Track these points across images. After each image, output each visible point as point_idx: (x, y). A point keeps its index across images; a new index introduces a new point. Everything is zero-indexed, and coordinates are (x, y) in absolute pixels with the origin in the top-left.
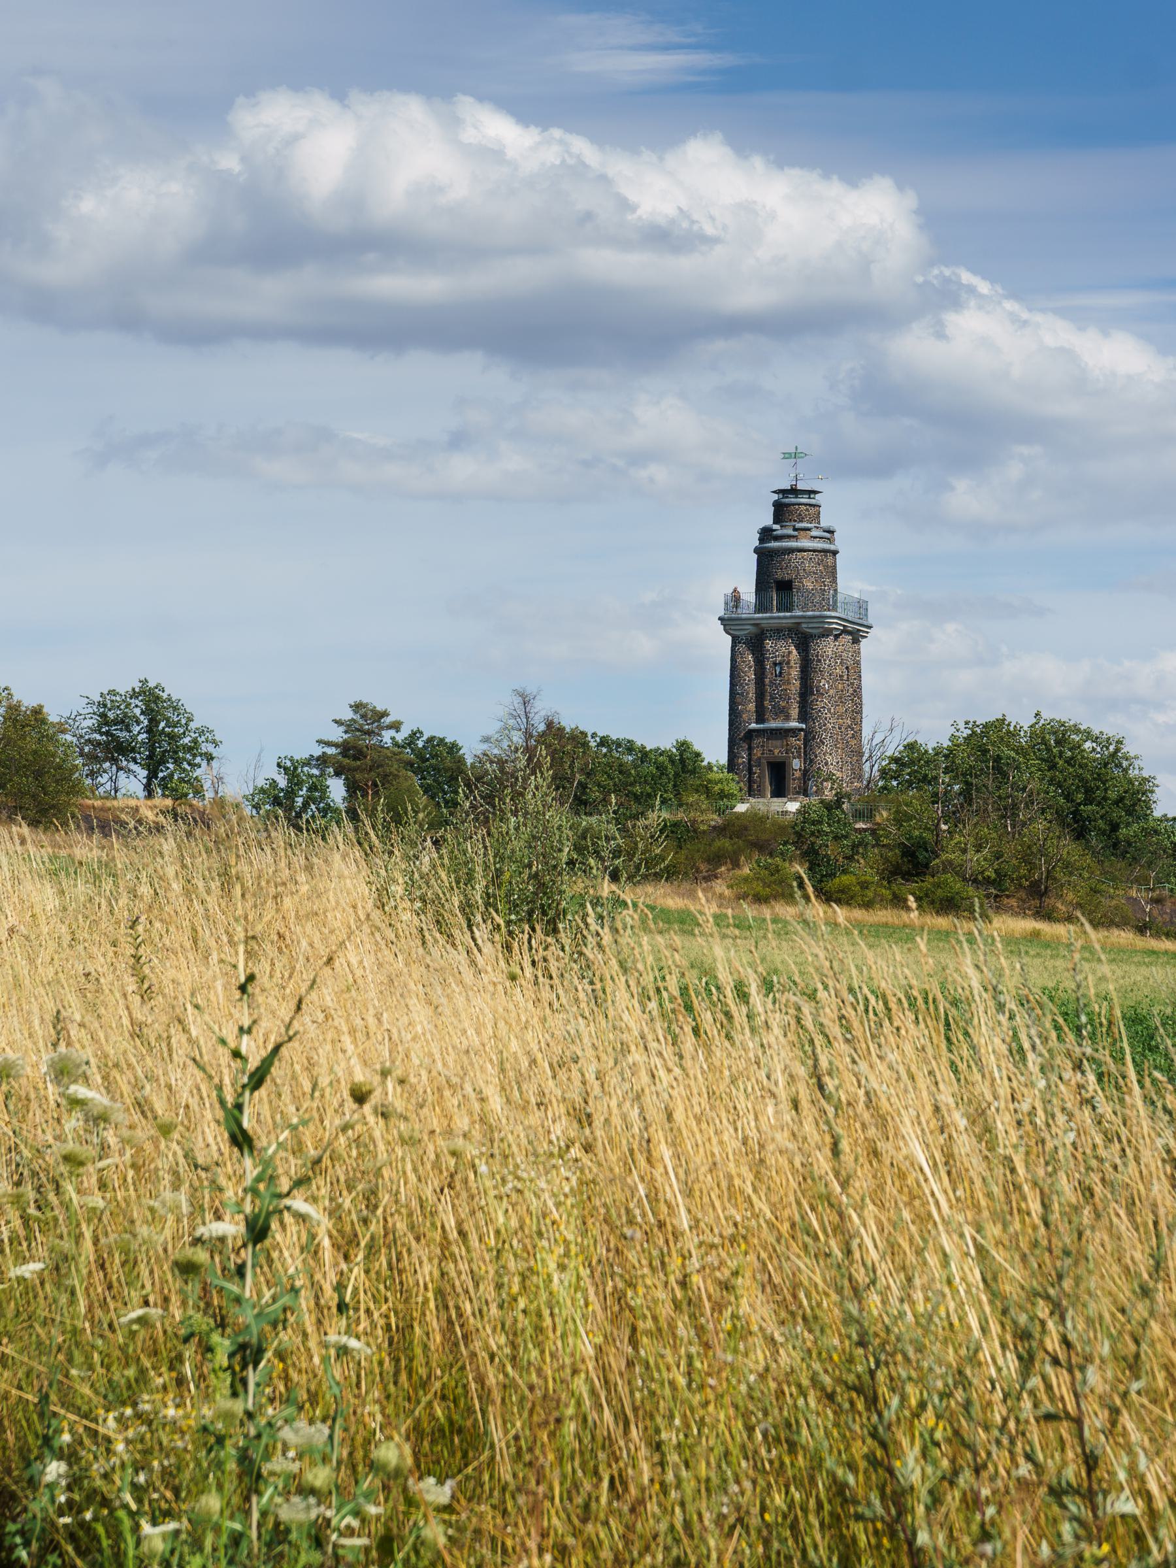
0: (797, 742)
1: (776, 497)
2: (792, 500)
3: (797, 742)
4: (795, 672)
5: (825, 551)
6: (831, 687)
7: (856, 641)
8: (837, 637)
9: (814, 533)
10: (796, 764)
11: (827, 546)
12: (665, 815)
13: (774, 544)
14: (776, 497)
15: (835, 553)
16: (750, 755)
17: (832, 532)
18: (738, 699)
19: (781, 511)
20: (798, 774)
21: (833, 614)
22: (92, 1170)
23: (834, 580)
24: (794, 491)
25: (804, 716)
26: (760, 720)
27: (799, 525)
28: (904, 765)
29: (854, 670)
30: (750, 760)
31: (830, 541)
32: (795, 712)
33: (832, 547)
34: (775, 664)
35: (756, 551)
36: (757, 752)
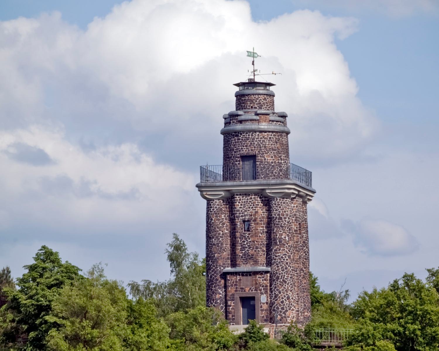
0: (263, 281)
1: (237, 89)
2: (251, 91)
3: (263, 281)
4: (262, 228)
5: (283, 132)
6: (290, 239)
7: (305, 203)
8: (292, 199)
9: (272, 118)
10: (264, 298)
11: (281, 128)
12: (413, 282)
13: (239, 127)
14: (237, 89)
15: (288, 133)
16: (226, 291)
17: (284, 116)
18: (214, 249)
19: (241, 99)
20: (265, 307)
21: (288, 181)
22: (416, 327)
23: (287, 156)
24: (252, 84)
25: (269, 263)
26: (234, 264)
27: (259, 112)
28: (411, 280)
29: (303, 226)
30: (226, 296)
31: (284, 123)
32: (262, 259)
33: (286, 129)
34: (244, 221)
35: (223, 133)
36: (231, 290)
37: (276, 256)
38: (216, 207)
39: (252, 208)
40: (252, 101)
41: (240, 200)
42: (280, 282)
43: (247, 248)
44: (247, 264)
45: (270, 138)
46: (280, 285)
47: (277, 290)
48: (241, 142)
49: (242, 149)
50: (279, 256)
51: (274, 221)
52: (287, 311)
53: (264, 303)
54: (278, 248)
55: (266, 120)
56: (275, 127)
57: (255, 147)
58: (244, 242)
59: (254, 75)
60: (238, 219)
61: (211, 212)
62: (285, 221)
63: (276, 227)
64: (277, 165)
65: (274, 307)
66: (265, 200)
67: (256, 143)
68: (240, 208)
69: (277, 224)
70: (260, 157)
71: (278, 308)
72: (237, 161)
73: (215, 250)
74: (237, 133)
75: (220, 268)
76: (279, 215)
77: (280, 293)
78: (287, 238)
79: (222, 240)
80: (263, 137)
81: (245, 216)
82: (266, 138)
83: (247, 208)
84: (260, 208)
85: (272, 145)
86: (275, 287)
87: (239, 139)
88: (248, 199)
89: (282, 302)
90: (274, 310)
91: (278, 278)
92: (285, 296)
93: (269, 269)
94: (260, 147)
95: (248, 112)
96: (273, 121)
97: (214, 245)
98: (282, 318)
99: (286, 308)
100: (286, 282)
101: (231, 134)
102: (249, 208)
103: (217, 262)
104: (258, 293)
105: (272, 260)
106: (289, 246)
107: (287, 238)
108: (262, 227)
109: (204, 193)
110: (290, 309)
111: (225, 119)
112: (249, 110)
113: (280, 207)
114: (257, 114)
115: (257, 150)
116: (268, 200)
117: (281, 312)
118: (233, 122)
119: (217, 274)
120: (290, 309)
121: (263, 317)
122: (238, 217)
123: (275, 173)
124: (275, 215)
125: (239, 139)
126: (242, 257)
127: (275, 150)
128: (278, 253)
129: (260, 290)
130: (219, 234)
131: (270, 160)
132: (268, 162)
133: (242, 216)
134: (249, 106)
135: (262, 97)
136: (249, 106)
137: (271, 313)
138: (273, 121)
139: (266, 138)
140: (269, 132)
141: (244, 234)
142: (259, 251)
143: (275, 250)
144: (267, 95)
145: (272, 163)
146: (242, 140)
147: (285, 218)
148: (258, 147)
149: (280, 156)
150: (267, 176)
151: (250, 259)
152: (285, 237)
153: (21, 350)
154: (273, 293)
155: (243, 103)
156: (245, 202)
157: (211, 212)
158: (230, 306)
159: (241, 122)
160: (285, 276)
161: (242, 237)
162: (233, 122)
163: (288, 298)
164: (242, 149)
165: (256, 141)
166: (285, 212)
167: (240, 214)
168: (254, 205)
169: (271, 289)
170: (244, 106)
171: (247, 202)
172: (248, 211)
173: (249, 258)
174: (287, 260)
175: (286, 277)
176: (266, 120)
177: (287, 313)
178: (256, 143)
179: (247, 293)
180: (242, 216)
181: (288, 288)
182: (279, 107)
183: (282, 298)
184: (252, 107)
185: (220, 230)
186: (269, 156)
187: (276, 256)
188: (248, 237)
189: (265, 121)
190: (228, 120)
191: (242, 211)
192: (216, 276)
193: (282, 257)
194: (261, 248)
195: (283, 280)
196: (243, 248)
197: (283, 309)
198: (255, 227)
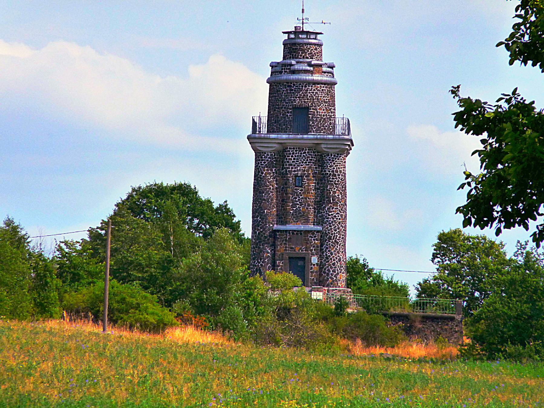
10: (315, 260)
20: (316, 268)
34: (296, 176)
37: (329, 215)
38: (267, 160)
39: (306, 163)
40: (303, 51)
41: (293, 153)
42: (332, 242)
43: (298, 204)
44: (297, 222)
45: (323, 90)
46: (332, 245)
47: (329, 251)
48: (293, 93)
49: (294, 100)
50: (332, 215)
51: (327, 177)
52: (338, 274)
53: (314, 265)
54: (331, 206)
55: (319, 71)
56: (327, 79)
57: (308, 99)
58: (296, 198)
59: (303, 23)
60: (290, 174)
61: (261, 165)
62: (339, 178)
63: (329, 184)
64: (327, 118)
65: (325, 269)
66: (318, 155)
67: (309, 95)
68: (293, 162)
69: (331, 181)
70: (313, 109)
71: (329, 271)
72: (288, 112)
73: (265, 205)
74: (289, 84)
75: (269, 225)
76: (333, 171)
77: (332, 254)
78: (340, 196)
79: (273, 195)
80: (317, 89)
81: (298, 171)
82: (319, 90)
83: (300, 163)
84: (313, 163)
85: (324, 97)
86: (327, 248)
87: (292, 90)
88: (301, 153)
89: (334, 264)
90: (325, 273)
91: (330, 238)
92: (336, 258)
93: (319, 228)
94: (313, 99)
95: (301, 62)
96: (325, 72)
97: (264, 200)
98: (333, 281)
99: (338, 271)
100: (338, 243)
101: (283, 84)
102: (303, 162)
103: (267, 219)
104: (308, 254)
105: (324, 219)
106: (342, 204)
107: (340, 196)
108: (314, 183)
109: (257, 145)
110: (341, 272)
111: (272, 67)
112: (301, 60)
113: (334, 164)
114: (310, 65)
115: (310, 102)
116: (321, 155)
117: (332, 275)
118: (285, 72)
119: (266, 231)
120: (341, 272)
121: (313, 279)
122: (290, 172)
123: (326, 126)
124: (329, 171)
125: (292, 90)
126: (293, 214)
127: (326, 103)
128: (331, 212)
129: (311, 250)
130: (270, 188)
131: (322, 112)
132: (319, 115)
133: (295, 171)
134: (301, 56)
135: (313, 47)
136: (301, 56)
137: (321, 275)
138: (325, 72)
139: (319, 90)
140: (322, 84)
141: (296, 189)
142: (310, 208)
143: (328, 209)
144: (318, 45)
145: (324, 116)
146: (295, 91)
147: (339, 175)
148: (311, 99)
149: (331, 109)
150: (318, 130)
151: (301, 216)
152: (339, 195)
153: (390, 407)
154: (324, 254)
155: (294, 52)
156: (298, 156)
157: (261, 165)
158: (279, 266)
159: (294, 72)
160: (337, 236)
161: (293, 193)
162: (285, 72)
163: (340, 260)
164: (294, 100)
165: (310, 93)
166: (339, 168)
167: (292, 168)
168: (307, 160)
169: (321, 251)
170: (295, 55)
171: (301, 156)
172: (302, 165)
173: (302, 217)
174: (340, 219)
175: (338, 238)
176: (319, 71)
177: (338, 277)
178: (309, 95)
179: (297, 253)
180: (295, 171)
181: (339, 249)
182: (326, 59)
183: (334, 260)
184: (304, 57)
185: (270, 185)
186: (320, 109)
187: (329, 215)
188: (300, 193)
189: (318, 73)
190: (278, 69)
191: (294, 165)
192: (264, 234)
193: (335, 216)
194: (312, 206)
195: (335, 241)
196: (294, 205)
197: (334, 271)
198: (308, 183)
